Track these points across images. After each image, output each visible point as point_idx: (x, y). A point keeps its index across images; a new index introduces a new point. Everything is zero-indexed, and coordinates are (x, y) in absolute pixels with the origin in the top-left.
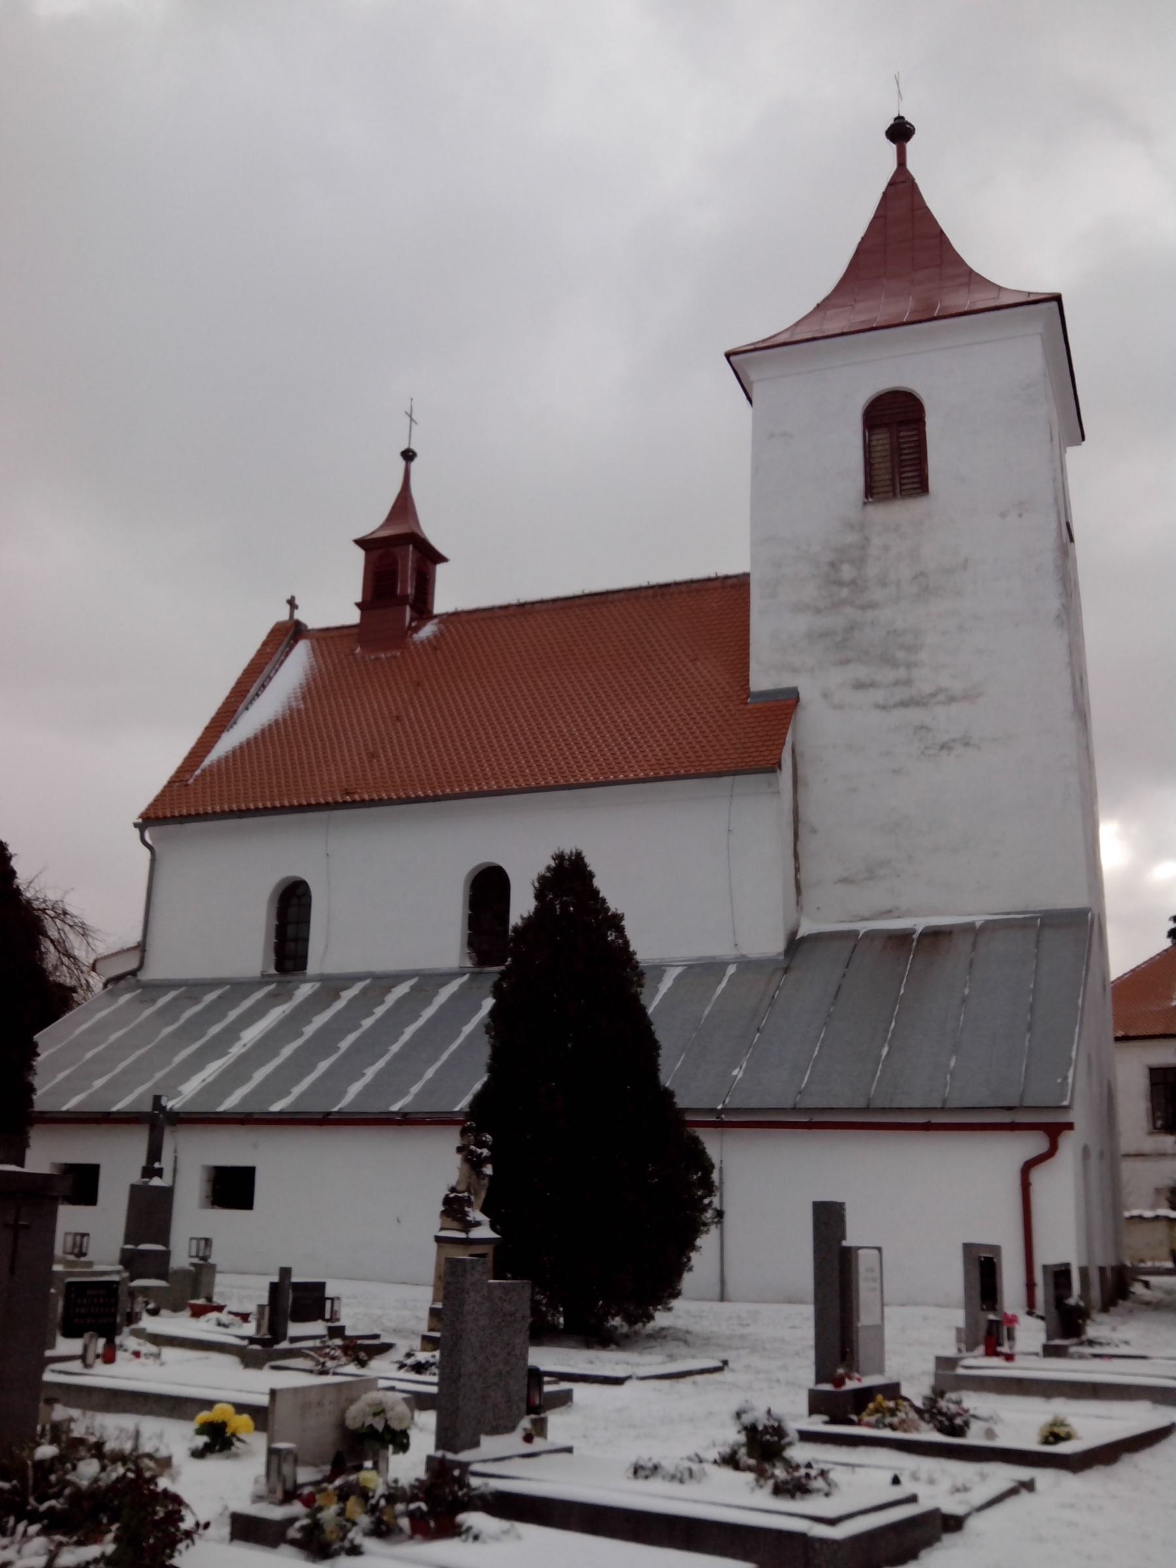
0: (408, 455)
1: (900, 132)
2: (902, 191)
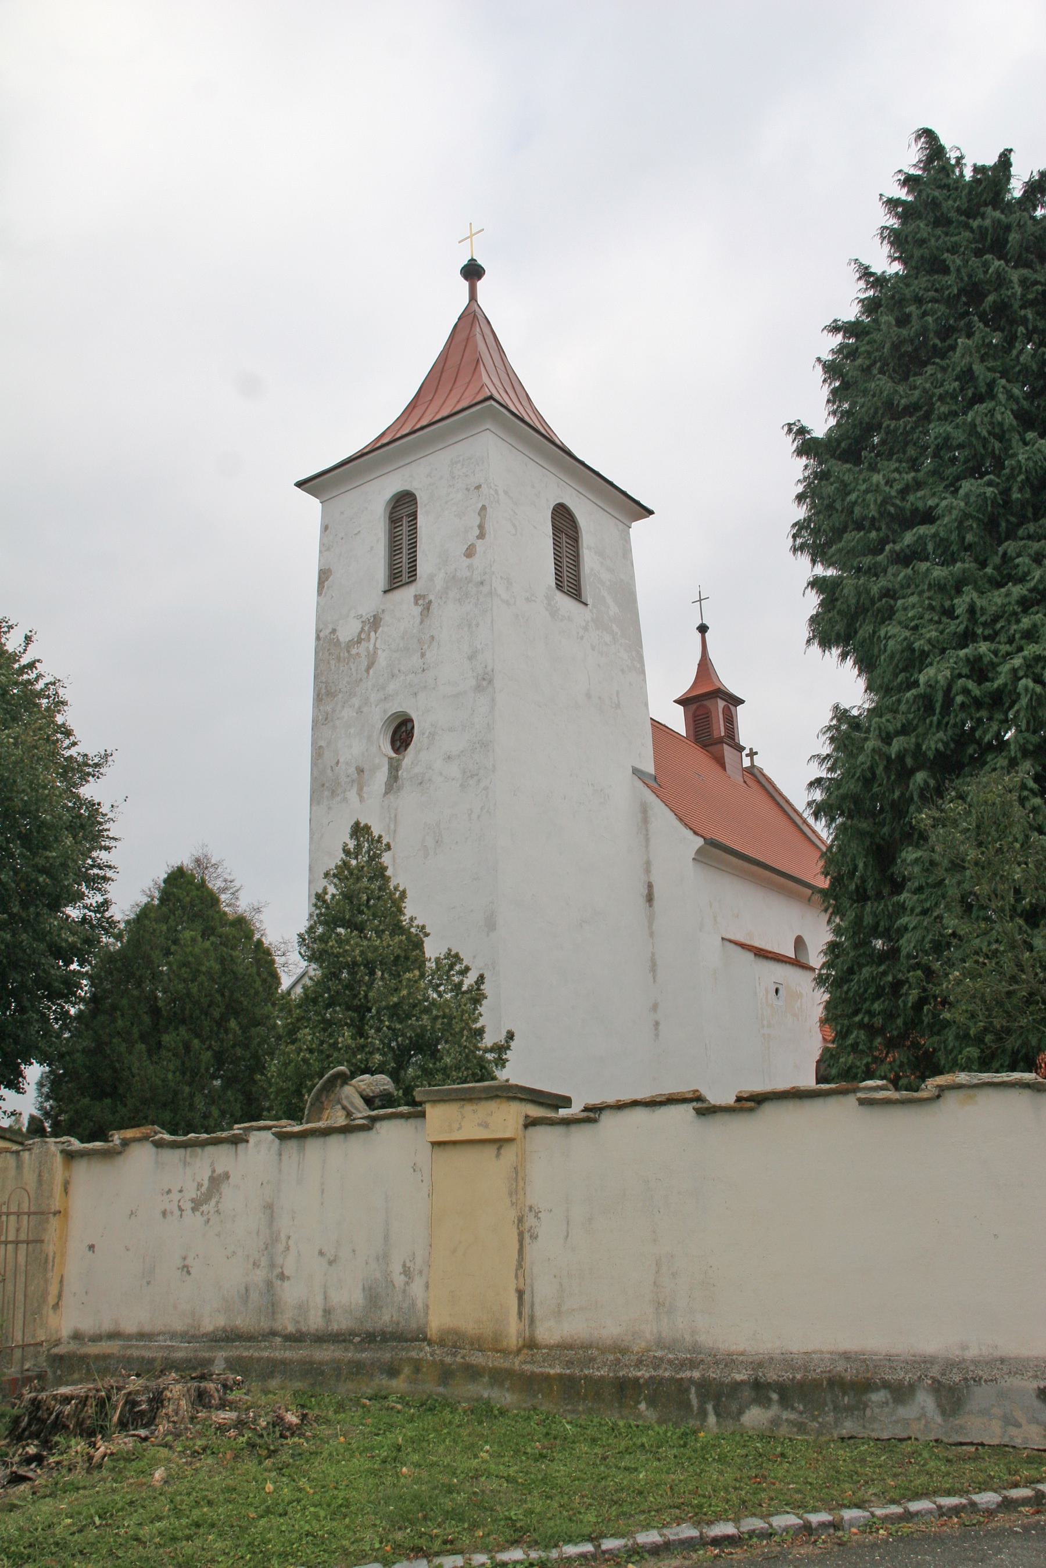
0: (703, 629)
1: (473, 272)
2: (471, 333)
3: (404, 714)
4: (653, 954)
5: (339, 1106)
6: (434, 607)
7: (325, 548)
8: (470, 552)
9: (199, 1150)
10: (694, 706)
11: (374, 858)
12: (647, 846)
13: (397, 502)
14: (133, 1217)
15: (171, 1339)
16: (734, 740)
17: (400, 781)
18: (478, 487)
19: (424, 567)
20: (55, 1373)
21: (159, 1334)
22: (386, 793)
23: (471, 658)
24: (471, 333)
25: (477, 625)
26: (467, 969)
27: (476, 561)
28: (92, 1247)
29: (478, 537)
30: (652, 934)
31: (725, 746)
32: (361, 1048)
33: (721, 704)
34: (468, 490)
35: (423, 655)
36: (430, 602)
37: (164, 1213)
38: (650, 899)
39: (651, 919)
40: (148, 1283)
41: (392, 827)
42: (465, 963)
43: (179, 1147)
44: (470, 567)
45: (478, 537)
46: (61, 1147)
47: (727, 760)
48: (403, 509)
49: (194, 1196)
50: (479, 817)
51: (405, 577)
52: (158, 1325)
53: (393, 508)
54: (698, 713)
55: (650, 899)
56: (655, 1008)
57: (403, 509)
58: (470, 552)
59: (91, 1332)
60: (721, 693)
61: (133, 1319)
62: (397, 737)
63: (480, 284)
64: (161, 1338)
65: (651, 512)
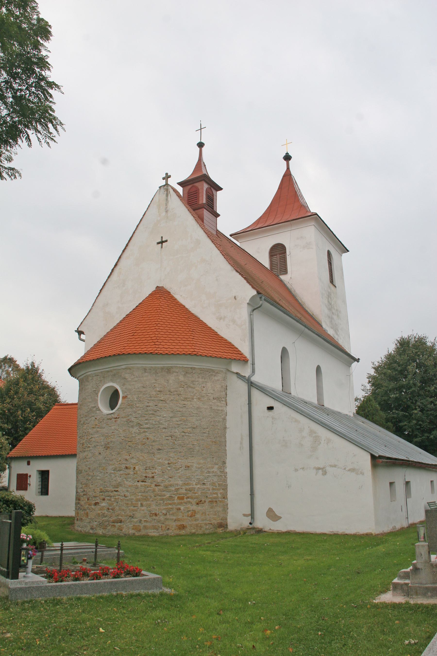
0: (201, 145)
1: (287, 158)
2: (288, 178)
5: (61, 543)
10: (189, 187)
16: (213, 209)
24: (288, 178)
31: (205, 210)
33: (206, 186)
47: (205, 217)
54: (190, 192)
60: (206, 178)
65: (348, 251)
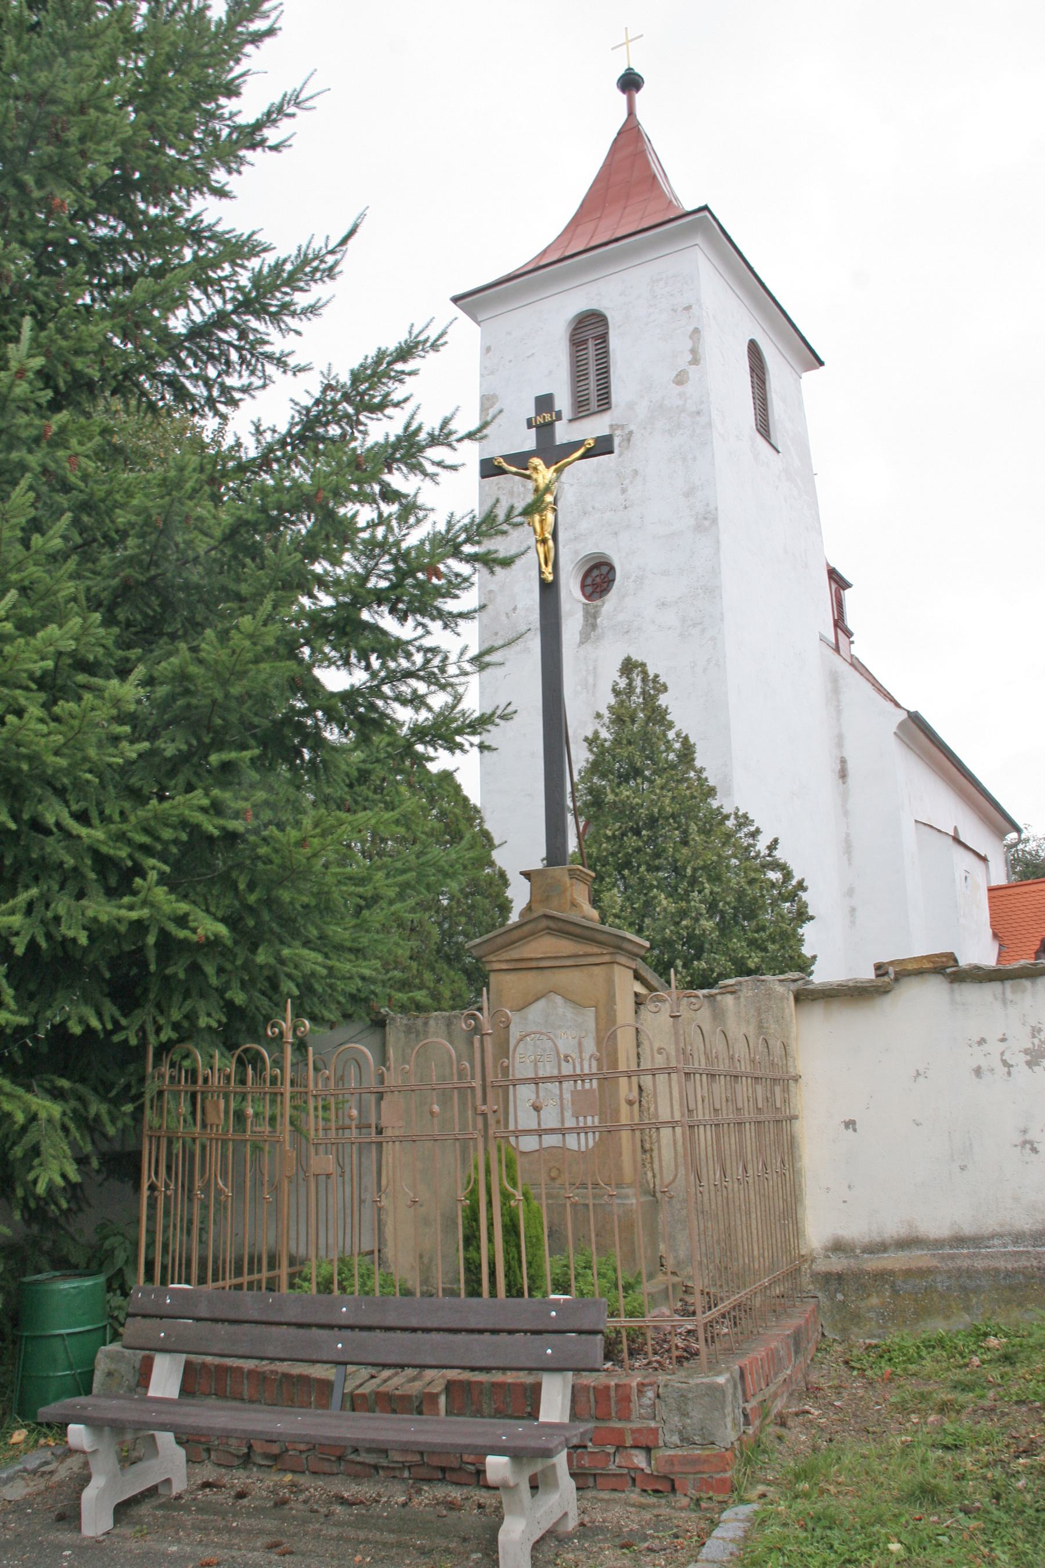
1: (630, 83)
3: (602, 555)
4: (848, 835)
6: (636, 438)
7: (487, 372)
8: (681, 379)
9: (1027, 983)
11: (649, 699)
12: (838, 720)
13: (580, 322)
14: (921, 1079)
15: (1015, 1243)
17: (599, 630)
18: (688, 308)
19: (614, 398)
20: (832, 1298)
21: (992, 1237)
22: (582, 643)
23: (687, 495)
25: (695, 459)
26: (758, 831)
27: (689, 388)
28: (850, 1124)
29: (690, 363)
30: (846, 813)
32: (683, 914)
34: (675, 311)
35: (624, 491)
36: (631, 433)
37: (978, 1072)
38: (843, 775)
39: (845, 797)
40: (963, 1168)
41: (591, 680)
42: (756, 825)
43: (991, 980)
44: (681, 395)
45: (690, 363)
46: (794, 987)
48: (590, 332)
49: (1030, 1046)
50: (705, 670)
51: (594, 405)
52: (990, 1224)
53: (575, 329)
55: (843, 775)
56: (850, 892)
57: (590, 332)
58: (681, 379)
59: (866, 1240)
61: (938, 1220)
62: (589, 581)
63: (639, 97)
64: (996, 1242)
65: (822, 364)
